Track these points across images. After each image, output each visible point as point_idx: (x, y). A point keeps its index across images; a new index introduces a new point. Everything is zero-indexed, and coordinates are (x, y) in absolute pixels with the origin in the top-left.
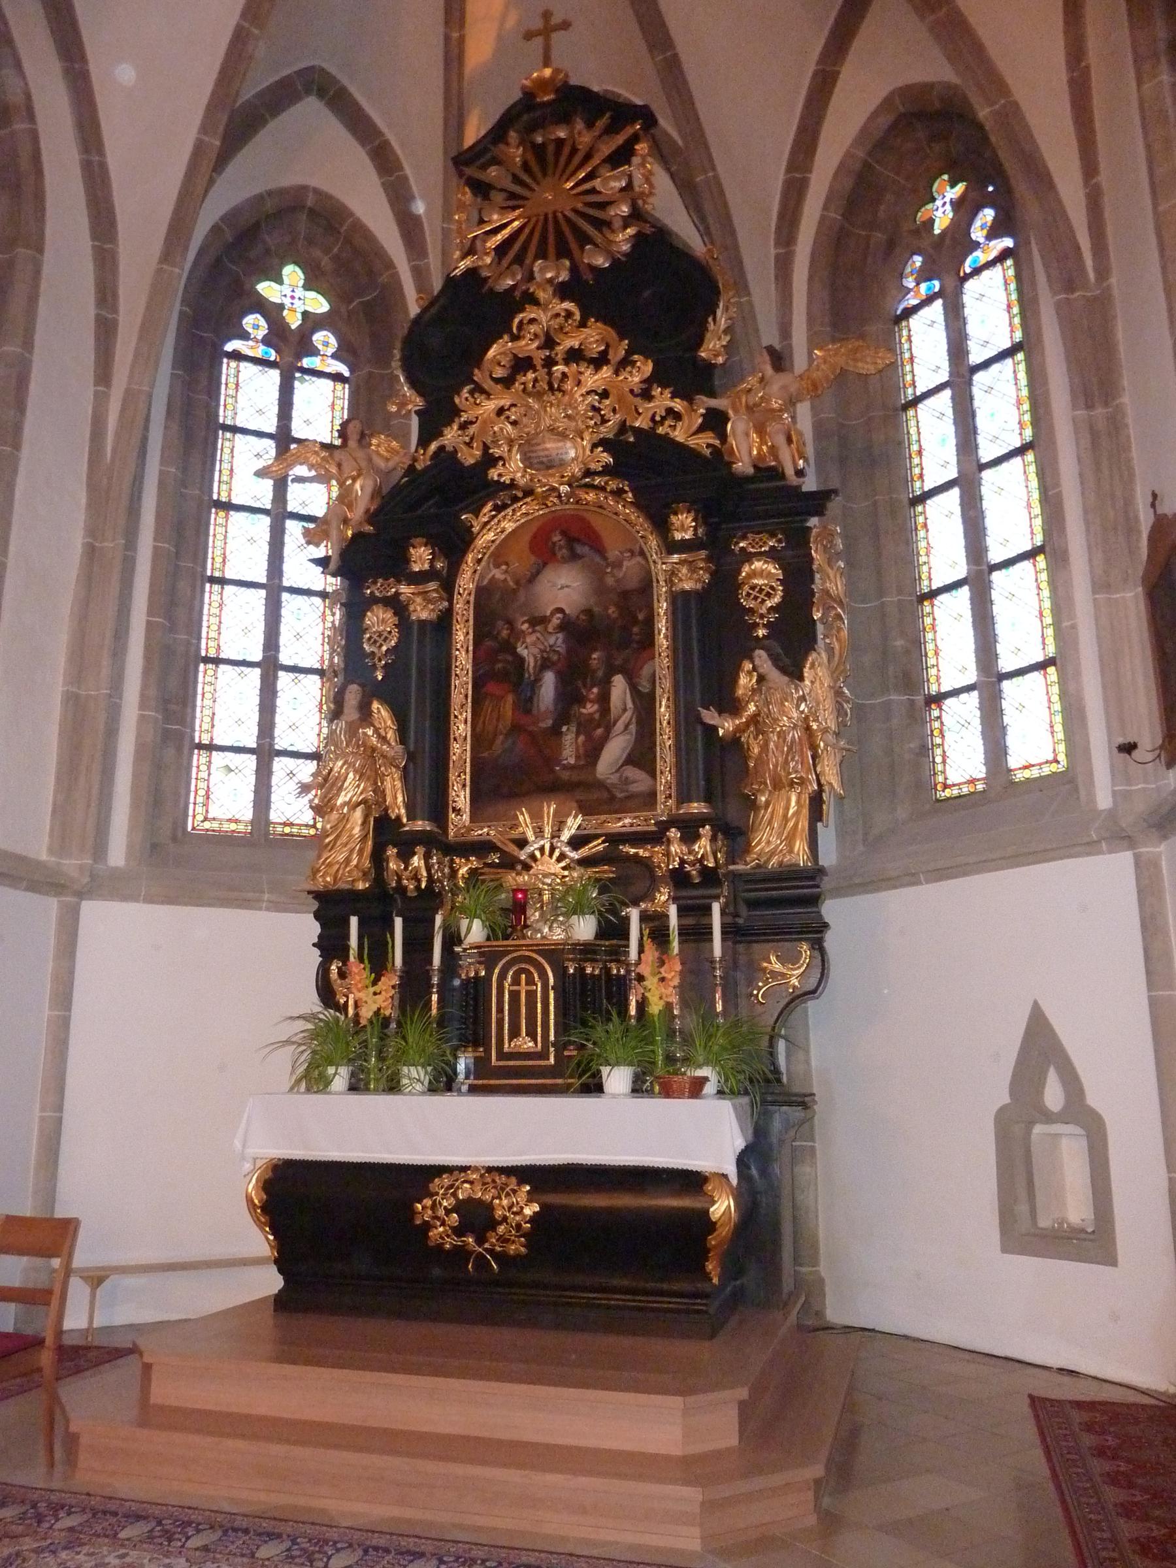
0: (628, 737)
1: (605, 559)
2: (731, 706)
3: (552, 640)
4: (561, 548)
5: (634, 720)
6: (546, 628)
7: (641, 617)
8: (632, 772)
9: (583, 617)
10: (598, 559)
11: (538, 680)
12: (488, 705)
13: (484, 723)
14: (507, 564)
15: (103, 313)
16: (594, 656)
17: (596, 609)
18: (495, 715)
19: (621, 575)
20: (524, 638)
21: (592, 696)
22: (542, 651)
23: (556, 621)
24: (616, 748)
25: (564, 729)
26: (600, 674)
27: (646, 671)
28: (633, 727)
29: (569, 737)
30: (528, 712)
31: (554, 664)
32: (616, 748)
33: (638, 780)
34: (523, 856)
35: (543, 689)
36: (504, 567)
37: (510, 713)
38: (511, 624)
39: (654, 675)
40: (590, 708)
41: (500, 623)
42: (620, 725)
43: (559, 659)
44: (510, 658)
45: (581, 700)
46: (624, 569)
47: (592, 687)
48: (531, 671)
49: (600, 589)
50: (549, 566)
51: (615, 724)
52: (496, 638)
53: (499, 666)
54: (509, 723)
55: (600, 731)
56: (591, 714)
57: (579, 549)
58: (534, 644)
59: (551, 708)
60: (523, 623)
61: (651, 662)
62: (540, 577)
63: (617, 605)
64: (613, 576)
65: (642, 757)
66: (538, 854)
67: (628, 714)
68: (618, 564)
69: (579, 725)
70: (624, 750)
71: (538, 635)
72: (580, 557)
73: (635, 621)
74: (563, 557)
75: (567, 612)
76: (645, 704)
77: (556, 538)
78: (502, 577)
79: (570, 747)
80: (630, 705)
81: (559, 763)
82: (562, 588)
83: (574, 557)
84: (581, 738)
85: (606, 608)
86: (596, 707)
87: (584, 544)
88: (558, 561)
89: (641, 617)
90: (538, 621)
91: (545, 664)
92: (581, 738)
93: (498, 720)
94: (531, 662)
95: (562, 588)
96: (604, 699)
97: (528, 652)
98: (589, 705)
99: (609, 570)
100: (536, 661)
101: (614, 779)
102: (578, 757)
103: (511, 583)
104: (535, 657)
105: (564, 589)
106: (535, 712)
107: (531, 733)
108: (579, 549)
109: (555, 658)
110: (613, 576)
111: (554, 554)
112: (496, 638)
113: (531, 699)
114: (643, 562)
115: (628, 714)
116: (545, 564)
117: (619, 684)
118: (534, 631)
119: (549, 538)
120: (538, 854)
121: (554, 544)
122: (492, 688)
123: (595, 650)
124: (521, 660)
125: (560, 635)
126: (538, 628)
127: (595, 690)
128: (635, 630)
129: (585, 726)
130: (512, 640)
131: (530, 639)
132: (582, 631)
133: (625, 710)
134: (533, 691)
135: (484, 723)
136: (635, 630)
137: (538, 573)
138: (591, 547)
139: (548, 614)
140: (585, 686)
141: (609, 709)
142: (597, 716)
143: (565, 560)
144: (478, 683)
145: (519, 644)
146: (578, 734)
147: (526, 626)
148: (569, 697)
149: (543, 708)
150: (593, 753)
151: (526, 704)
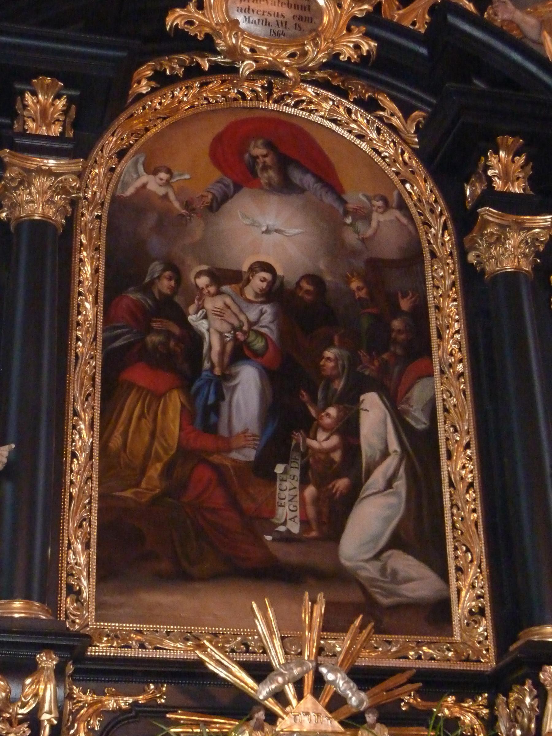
0: (393, 500)
1: (344, 202)
2: (99, 721)
3: (253, 315)
4: (265, 168)
5: (402, 471)
6: (242, 292)
7: (405, 304)
8: (404, 563)
9: (306, 286)
10: (329, 199)
11: (227, 376)
12: (132, 406)
13: (125, 433)
14: (169, 171)
15: (79, 666)
16: (329, 354)
17: (328, 278)
18: (146, 425)
19: (370, 232)
20: (201, 298)
21: (327, 421)
22: (234, 329)
23: (259, 282)
24: (373, 517)
25: (279, 469)
26: (339, 385)
27: (418, 394)
28: (401, 484)
29: (287, 485)
30: (211, 429)
31: (257, 354)
32: (373, 517)
33: (416, 579)
34: (263, 692)
35: (238, 395)
36: (163, 175)
37: (175, 428)
38: (176, 272)
39: (433, 400)
40: (324, 441)
41: (156, 267)
42: (378, 478)
43: (267, 346)
44: (176, 330)
45: (309, 426)
46: (374, 224)
47: (327, 405)
48: (215, 357)
49: (335, 246)
50: (245, 190)
51: (369, 473)
52: (147, 289)
53: (153, 339)
54: (174, 443)
55: (342, 483)
56: (328, 452)
57: (297, 176)
58: (220, 314)
59: (254, 428)
60: (199, 274)
61: (426, 381)
62: (228, 205)
63: (364, 279)
64: (357, 232)
65: (421, 532)
66: (290, 691)
67: (391, 462)
68: (365, 216)
69: (304, 469)
70: (387, 520)
71: (229, 301)
72: (301, 190)
73: (396, 312)
74: (270, 184)
75: (280, 272)
76: (421, 451)
77: (258, 150)
78: (161, 191)
79: (289, 504)
80: (394, 445)
81: (272, 528)
82: (267, 232)
83: (286, 187)
84: (310, 491)
85: (348, 282)
86: (335, 440)
87: (306, 171)
88: (261, 188)
89: (405, 304)
90: (225, 278)
91: (239, 352)
92: (310, 491)
93: (153, 435)
94: (213, 344)
95: (267, 232)
96: (349, 429)
97: (211, 322)
98: (322, 435)
99: (349, 220)
100: (223, 345)
101: (370, 571)
102: (305, 522)
103: (177, 205)
104: (222, 336)
105: (271, 233)
106: (223, 431)
107: (216, 468)
108: (297, 176)
109: (259, 344)
110: (357, 232)
111: (254, 174)
112: (147, 289)
113: (216, 409)
114: (404, 220)
115: (391, 462)
116: (238, 187)
117: (373, 412)
118: (219, 293)
119: (243, 148)
120: (290, 691)
121: (255, 158)
122: (139, 375)
123: (330, 344)
124: (195, 339)
125: (267, 308)
126: (225, 288)
127: (332, 411)
128: (397, 324)
129: (316, 471)
130: (178, 299)
131: (211, 304)
132: (303, 306)
133: (385, 454)
134: (220, 397)
135: (125, 433)
136: (397, 324)
137: (225, 198)
138: (319, 179)
139: (245, 268)
140: (314, 400)
141: (358, 448)
142: (337, 456)
143: (272, 188)
144: (114, 364)
145: (192, 309)
146: (304, 482)
147: (203, 281)
148: (285, 417)
149: (238, 428)
150: (333, 516)
151: (207, 413)
